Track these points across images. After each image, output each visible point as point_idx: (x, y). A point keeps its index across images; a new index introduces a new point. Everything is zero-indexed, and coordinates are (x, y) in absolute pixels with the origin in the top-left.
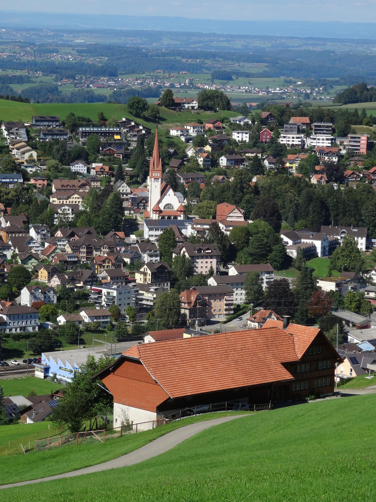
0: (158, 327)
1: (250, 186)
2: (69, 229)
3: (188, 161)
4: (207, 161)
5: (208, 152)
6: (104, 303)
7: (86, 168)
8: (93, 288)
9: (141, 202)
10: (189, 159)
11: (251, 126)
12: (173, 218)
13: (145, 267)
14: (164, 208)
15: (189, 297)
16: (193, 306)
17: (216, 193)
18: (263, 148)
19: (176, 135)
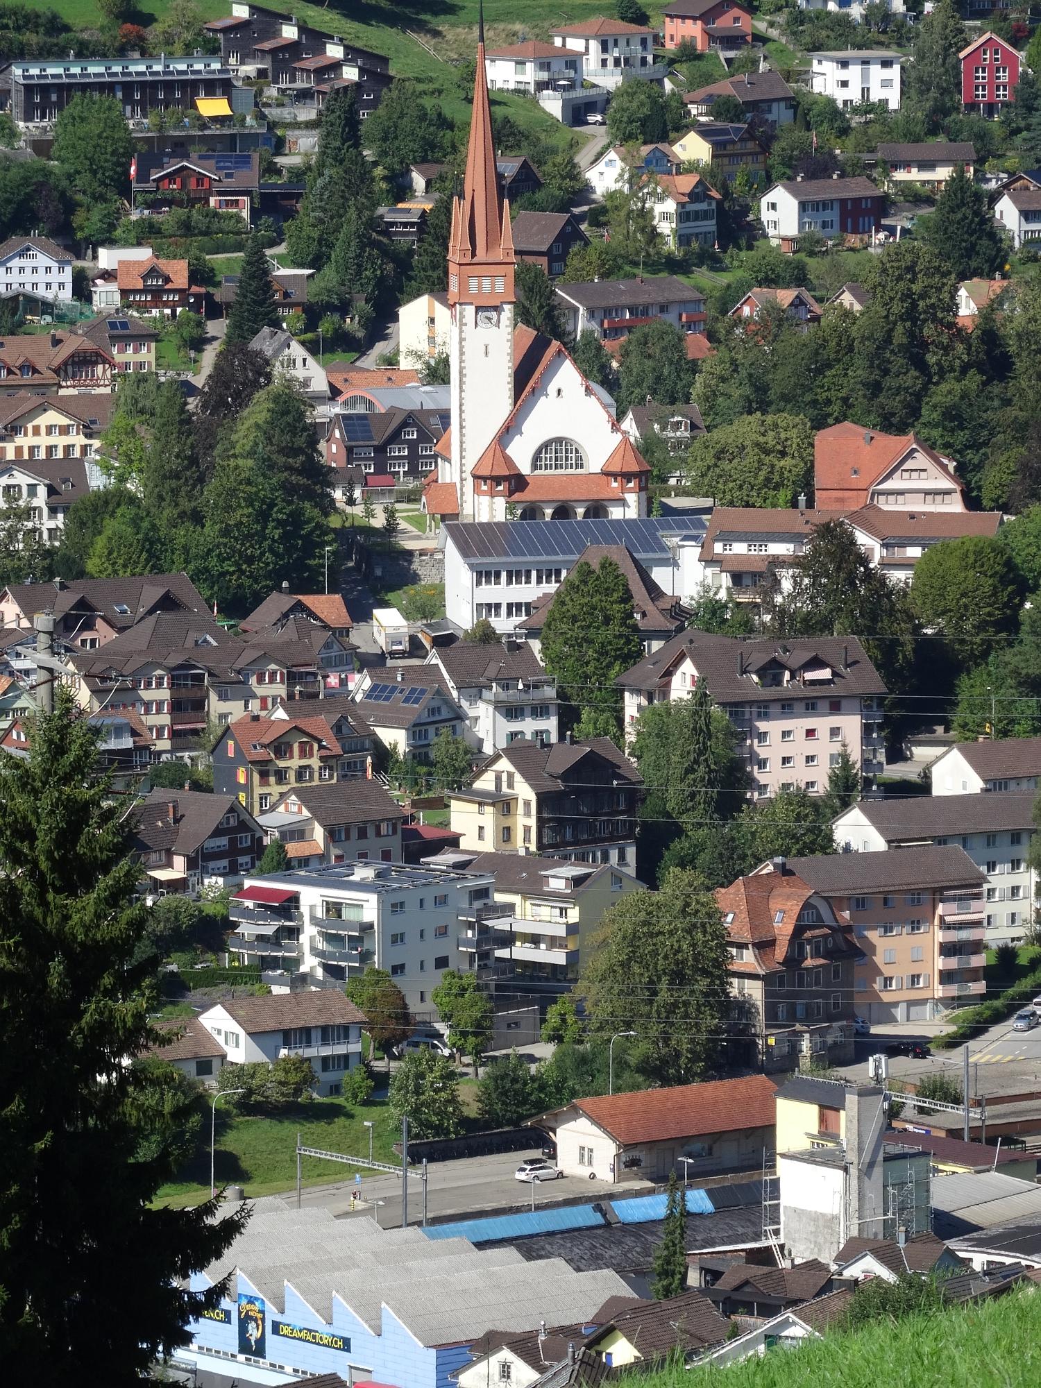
0: (617, 1076)
1: (959, 334)
2: (63, 587)
3: (599, 216)
4: (697, 216)
5: (692, 167)
6: (310, 963)
7: (67, 276)
8: (248, 883)
9: (395, 437)
10: (603, 210)
11: (903, 25)
12: (586, 515)
13: (504, 765)
14: (536, 461)
15: (758, 913)
16: (787, 961)
17: (780, 380)
18: (981, 137)
19: (512, 86)
